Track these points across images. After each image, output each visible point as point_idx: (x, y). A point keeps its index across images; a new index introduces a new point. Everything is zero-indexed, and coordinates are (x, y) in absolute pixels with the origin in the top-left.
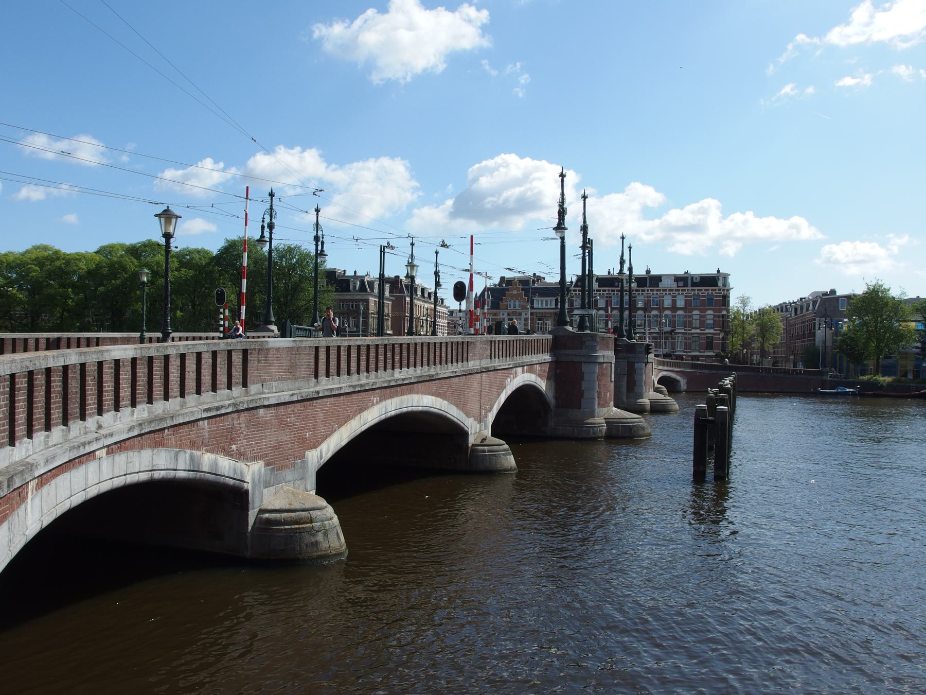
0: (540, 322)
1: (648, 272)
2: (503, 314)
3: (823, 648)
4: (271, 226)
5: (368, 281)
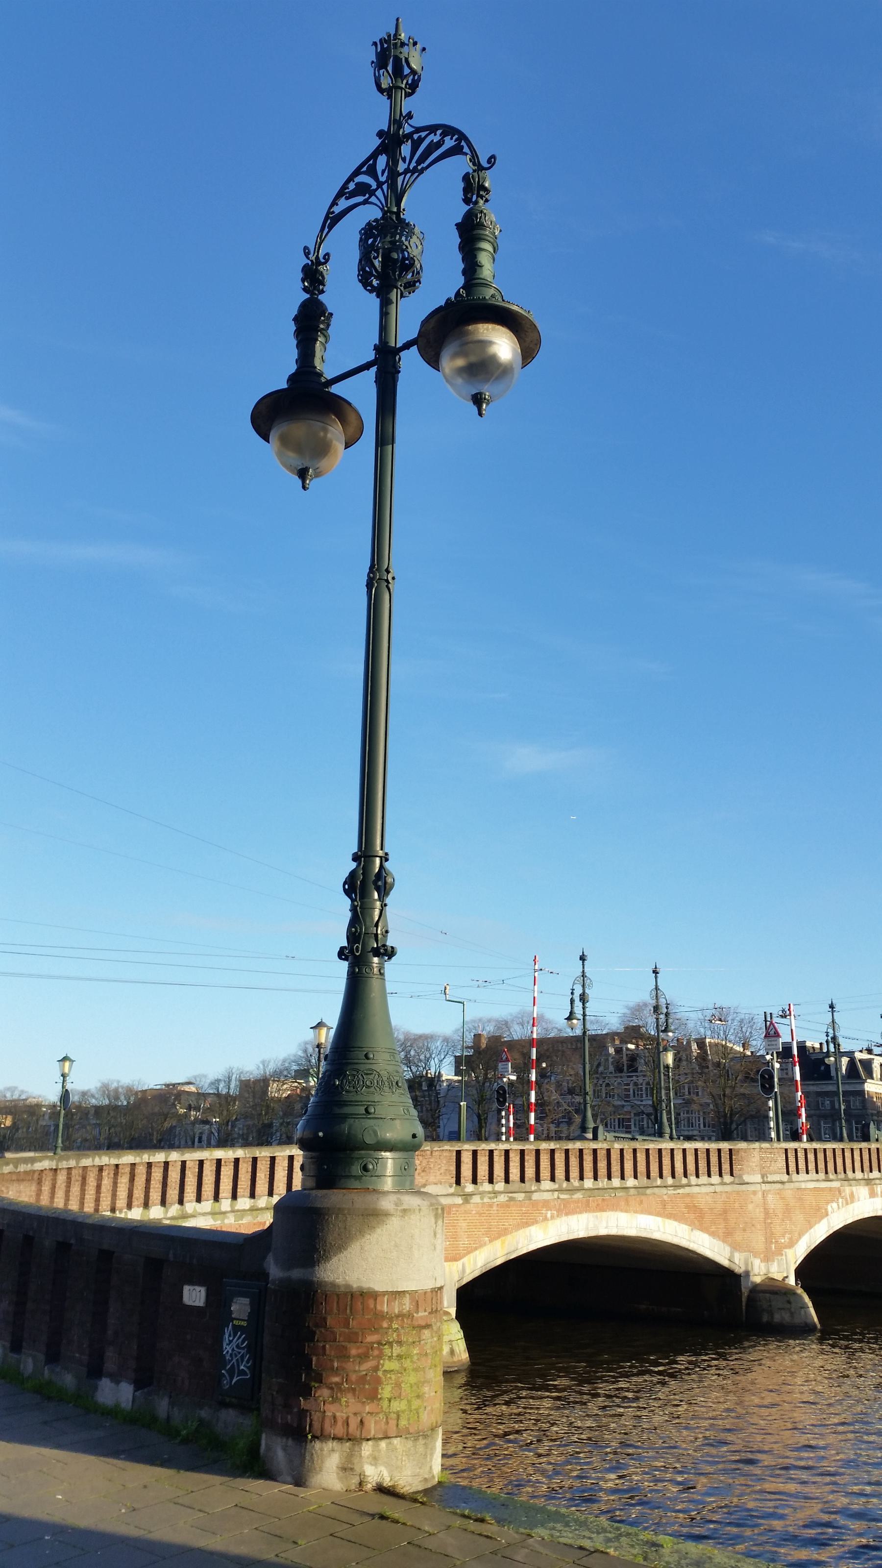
3: (786, 1483)
4: (583, 998)
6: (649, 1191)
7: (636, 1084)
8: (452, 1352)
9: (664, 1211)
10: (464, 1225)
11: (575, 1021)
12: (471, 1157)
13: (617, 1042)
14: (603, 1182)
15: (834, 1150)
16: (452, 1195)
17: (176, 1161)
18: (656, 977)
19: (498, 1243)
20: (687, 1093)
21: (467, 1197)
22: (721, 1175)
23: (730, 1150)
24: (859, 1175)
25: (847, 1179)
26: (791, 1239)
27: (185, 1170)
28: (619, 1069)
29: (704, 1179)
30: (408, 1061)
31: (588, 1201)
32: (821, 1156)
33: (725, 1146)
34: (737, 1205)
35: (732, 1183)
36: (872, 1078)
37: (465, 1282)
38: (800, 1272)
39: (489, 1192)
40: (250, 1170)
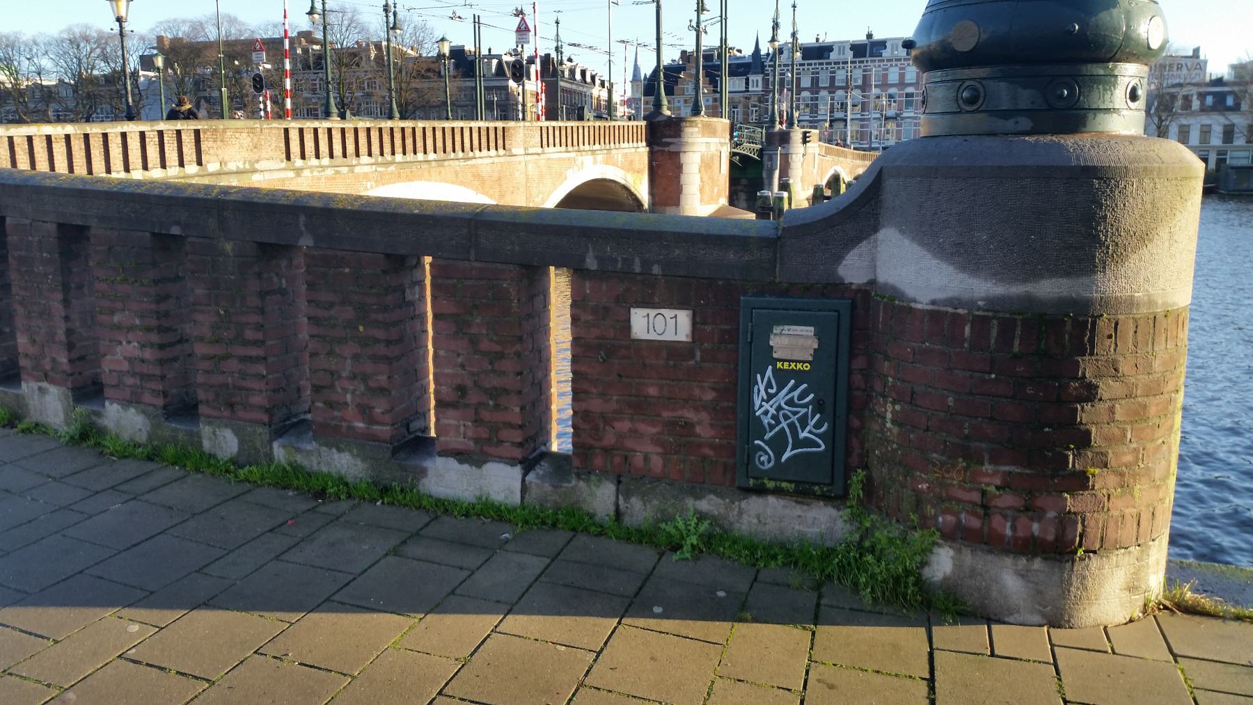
1: (869, 36)
2: (679, 102)
6: (446, 163)
9: (457, 180)
11: (316, 16)
20: (366, 87)
21: (298, 171)
22: (497, 149)
23: (504, 128)
27: (14, 147)
29: (485, 152)
31: (399, 173)
33: (500, 124)
35: (504, 155)
39: (317, 167)
40: (83, 147)
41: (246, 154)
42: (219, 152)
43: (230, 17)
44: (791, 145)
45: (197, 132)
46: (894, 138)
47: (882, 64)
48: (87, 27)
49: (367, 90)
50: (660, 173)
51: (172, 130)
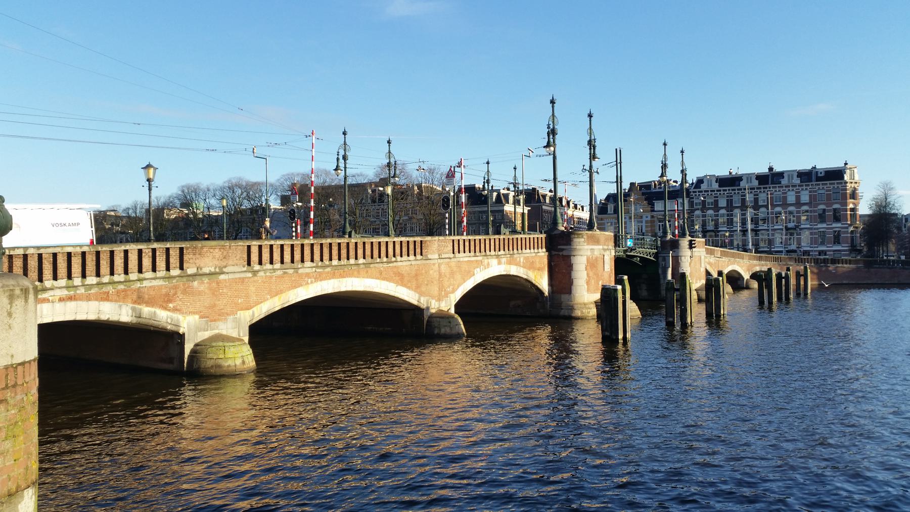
0: (661, 224)
1: (771, 169)
5: (542, 195)
6: (372, 266)
7: (383, 209)
8: (244, 362)
9: (381, 276)
10: (253, 289)
11: (339, 171)
12: (258, 249)
13: (373, 186)
14: (344, 261)
15: (480, 240)
16: (245, 271)
17: (33, 254)
18: (389, 146)
19: (276, 299)
21: (255, 273)
22: (415, 255)
23: (421, 241)
24: (493, 253)
25: (486, 255)
26: (453, 288)
28: (374, 201)
30: (249, 198)
31: (334, 273)
32: (472, 243)
34: (423, 272)
36: (508, 203)
37: (254, 321)
38: (458, 306)
39: (270, 270)
41: (217, 263)
42: (197, 261)
43: (326, 171)
44: (680, 250)
45: (181, 249)
46: (795, 243)
47: (781, 189)
48: (240, 179)
49: (410, 215)
50: (557, 270)
51: (163, 248)
